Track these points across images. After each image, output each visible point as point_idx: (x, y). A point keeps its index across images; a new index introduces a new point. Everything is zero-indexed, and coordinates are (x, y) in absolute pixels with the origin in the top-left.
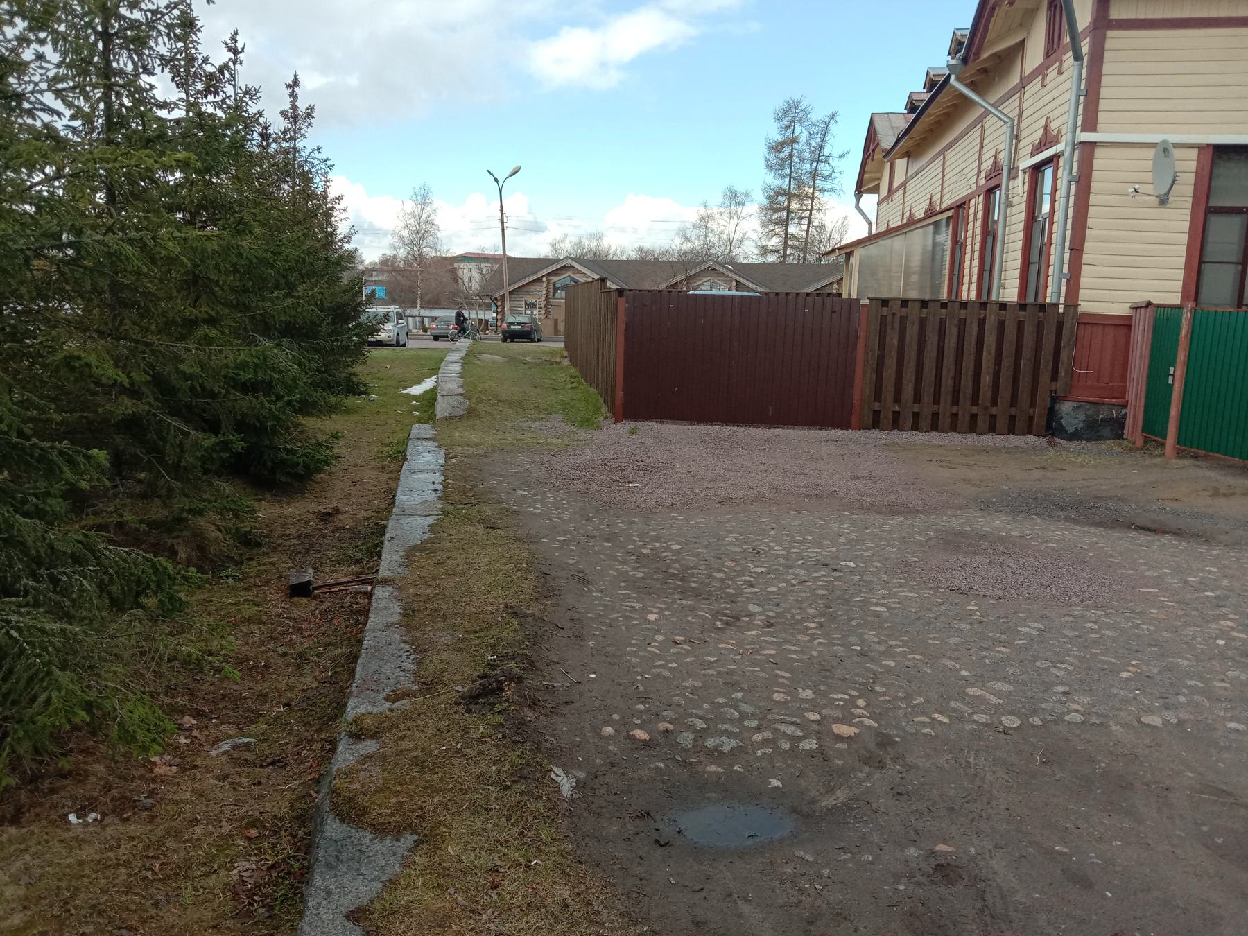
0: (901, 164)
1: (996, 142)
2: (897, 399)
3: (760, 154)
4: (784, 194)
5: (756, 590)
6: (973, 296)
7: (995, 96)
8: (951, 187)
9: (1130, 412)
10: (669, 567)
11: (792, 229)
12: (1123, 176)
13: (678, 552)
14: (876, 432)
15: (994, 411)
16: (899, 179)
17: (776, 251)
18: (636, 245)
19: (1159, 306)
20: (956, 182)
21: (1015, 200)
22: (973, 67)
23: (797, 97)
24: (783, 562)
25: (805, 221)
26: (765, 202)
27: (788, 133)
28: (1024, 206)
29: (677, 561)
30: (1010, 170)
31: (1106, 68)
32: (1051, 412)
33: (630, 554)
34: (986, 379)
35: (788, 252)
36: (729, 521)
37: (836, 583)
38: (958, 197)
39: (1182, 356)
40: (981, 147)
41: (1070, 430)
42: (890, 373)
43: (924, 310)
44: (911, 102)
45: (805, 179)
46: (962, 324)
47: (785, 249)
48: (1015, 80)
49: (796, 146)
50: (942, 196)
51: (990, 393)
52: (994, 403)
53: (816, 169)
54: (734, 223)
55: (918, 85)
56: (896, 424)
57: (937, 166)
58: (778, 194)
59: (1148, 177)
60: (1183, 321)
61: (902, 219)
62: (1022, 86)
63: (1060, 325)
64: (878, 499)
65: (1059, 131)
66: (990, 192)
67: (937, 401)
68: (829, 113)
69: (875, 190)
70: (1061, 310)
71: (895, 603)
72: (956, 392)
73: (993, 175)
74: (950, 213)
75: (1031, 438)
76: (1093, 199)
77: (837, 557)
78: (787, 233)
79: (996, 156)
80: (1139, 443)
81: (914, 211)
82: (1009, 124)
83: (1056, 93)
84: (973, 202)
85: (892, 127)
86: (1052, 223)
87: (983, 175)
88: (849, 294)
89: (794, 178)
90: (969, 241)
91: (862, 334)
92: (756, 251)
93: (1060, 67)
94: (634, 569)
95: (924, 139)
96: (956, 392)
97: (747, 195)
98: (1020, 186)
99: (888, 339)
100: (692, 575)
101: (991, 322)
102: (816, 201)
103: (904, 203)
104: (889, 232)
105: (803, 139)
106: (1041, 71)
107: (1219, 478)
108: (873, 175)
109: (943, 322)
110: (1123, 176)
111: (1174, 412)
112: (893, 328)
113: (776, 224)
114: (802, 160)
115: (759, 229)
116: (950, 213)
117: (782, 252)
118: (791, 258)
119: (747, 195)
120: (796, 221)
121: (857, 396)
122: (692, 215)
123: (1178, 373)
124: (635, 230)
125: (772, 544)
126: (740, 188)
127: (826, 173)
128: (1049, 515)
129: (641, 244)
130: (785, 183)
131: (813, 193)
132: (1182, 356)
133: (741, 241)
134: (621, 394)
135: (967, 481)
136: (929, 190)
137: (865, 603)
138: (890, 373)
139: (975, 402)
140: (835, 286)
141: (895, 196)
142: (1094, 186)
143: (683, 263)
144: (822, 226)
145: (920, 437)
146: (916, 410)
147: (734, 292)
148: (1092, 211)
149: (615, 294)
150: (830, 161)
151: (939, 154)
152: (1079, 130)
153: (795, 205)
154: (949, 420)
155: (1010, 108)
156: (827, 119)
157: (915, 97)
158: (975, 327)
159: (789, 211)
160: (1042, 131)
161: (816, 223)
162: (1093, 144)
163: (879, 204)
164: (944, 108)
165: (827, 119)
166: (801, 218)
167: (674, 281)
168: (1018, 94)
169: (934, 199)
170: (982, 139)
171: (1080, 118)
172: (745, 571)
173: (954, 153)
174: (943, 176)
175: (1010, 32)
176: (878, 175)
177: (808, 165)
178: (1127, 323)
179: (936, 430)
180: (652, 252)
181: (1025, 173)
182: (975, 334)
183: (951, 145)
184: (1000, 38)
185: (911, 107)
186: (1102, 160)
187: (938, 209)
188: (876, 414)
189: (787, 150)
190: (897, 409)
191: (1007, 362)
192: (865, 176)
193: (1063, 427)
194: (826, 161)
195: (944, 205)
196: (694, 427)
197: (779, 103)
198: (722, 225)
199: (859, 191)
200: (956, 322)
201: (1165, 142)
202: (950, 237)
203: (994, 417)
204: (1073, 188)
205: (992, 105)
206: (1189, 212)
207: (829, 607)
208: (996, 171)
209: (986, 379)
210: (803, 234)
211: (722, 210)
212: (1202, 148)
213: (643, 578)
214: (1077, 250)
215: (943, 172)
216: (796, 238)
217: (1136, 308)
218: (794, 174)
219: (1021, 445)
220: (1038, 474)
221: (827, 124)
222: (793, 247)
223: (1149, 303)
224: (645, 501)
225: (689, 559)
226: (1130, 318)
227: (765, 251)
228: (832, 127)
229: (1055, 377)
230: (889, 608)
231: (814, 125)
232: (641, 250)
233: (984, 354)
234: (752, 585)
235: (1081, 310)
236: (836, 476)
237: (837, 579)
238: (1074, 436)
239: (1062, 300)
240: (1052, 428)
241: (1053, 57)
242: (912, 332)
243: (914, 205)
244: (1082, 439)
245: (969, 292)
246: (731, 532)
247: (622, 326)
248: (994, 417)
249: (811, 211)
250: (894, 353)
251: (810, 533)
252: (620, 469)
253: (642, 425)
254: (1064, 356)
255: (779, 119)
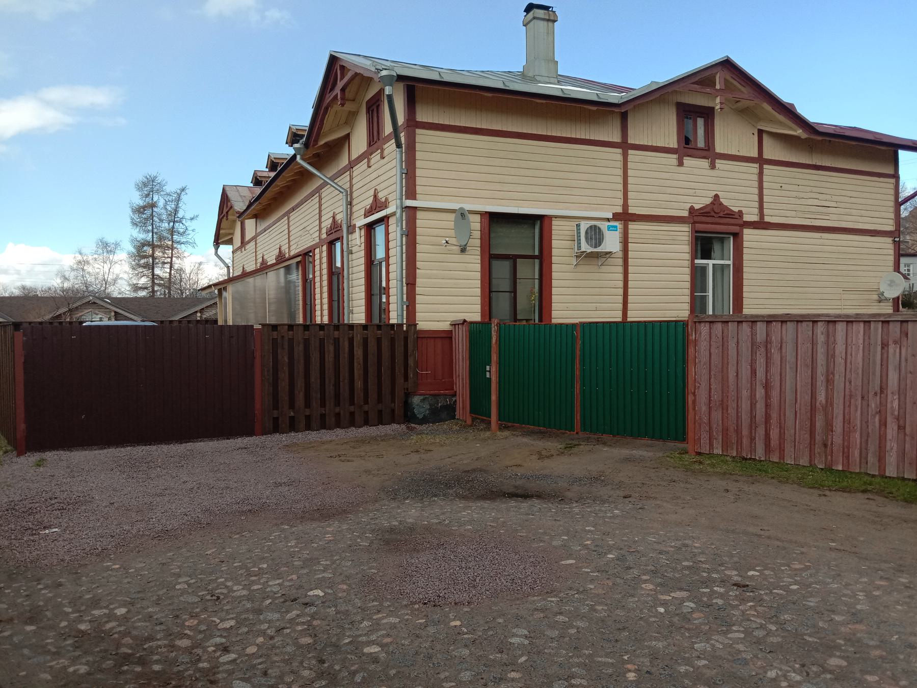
0: (250, 224)
1: (332, 207)
2: (292, 406)
3: (127, 214)
4: (149, 245)
5: (233, 656)
6: (326, 320)
7: (333, 170)
8: (297, 240)
9: (459, 399)
10: (118, 645)
11: (157, 271)
12: (436, 232)
13: (125, 618)
14: (277, 436)
15: (366, 408)
16: (249, 235)
17: (146, 288)
18: (19, 284)
19: (471, 323)
20: (301, 236)
21: (354, 249)
22: (311, 152)
23: (154, 174)
24: (249, 605)
25: (168, 266)
26: (134, 250)
27: (148, 200)
28: (362, 253)
29: (126, 634)
30: (348, 227)
31: (418, 155)
32: (407, 405)
33: (63, 636)
34: (359, 384)
35: (156, 289)
36: (172, 560)
37: (315, 623)
38: (304, 247)
39: (494, 357)
40: (320, 211)
41: (420, 416)
42: (284, 385)
43: (307, 332)
44: (256, 178)
45: (165, 234)
46: (337, 342)
47: (153, 287)
48: (344, 162)
49: (155, 209)
50: (289, 247)
51: (362, 395)
52: (366, 402)
53: (173, 227)
54: (107, 267)
55: (262, 166)
56: (293, 427)
57: (283, 224)
58: (143, 245)
59: (452, 233)
60: (493, 333)
61: (256, 264)
62: (351, 165)
63: (406, 339)
64: (307, 505)
65: (386, 199)
66: (331, 244)
67: (323, 405)
68: (180, 187)
69: (230, 242)
70: (405, 329)
71: (383, 636)
72: (337, 396)
73: (333, 231)
74: (299, 259)
75: (395, 426)
76: (419, 248)
77: (301, 587)
78: (153, 274)
79: (334, 218)
80: (469, 422)
81: (265, 257)
82: (344, 194)
83: (380, 172)
84: (317, 251)
85: (241, 196)
86: (388, 265)
87: (324, 231)
88: (226, 321)
89: (156, 233)
90: (317, 279)
91: (258, 354)
92: (128, 288)
93: (382, 153)
94: (74, 661)
95: (269, 205)
96: (337, 396)
97: (117, 245)
98: (358, 239)
99: (280, 357)
100: (152, 651)
101: (358, 340)
102: (175, 251)
103: (256, 252)
104: (245, 275)
105: (161, 203)
106: (366, 156)
107: (532, 442)
108: (227, 231)
109: (322, 341)
110: (436, 232)
111: (494, 398)
112: (283, 348)
113: (144, 267)
114: (161, 221)
115: (131, 271)
116: (299, 259)
117: (151, 289)
118: (159, 293)
119: (117, 245)
120: (160, 265)
121: (258, 406)
122: (68, 260)
123: (494, 369)
124: (18, 272)
125: (229, 584)
126: (110, 239)
127: (182, 231)
128: (444, 495)
129: (24, 283)
130: (149, 237)
131: (172, 245)
132: (494, 357)
133: (115, 281)
134: (22, 426)
135: (368, 472)
136: (277, 242)
137: (356, 645)
138: (284, 385)
139: (352, 402)
140: (199, 314)
141: (247, 247)
142: (419, 239)
143: (65, 298)
144: (180, 271)
145: (313, 436)
146: (307, 414)
147: (113, 323)
148: (419, 256)
149: (10, 330)
150: (184, 222)
151: (284, 216)
152: (404, 197)
153: (158, 253)
154: (333, 419)
155: (344, 180)
156: (179, 191)
157: (259, 174)
158: (346, 344)
159: (154, 258)
160: (372, 199)
161: (176, 266)
162: (415, 208)
163: (233, 252)
164: (288, 182)
165: (179, 191)
166: (164, 263)
167: (58, 313)
168: (348, 173)
169: (283, 249)
170: (320, 206)
171: (404, 189)
172: (212, 626)
173: (297, 214)
174: (289, 232)
175: (338, 127)
176: (231, 231)
177: (166, 225)
178: (450, 336)
179: (325, 428)
180: (35, 290)
181: (360, 229)
182: (347, 350)
183: (293, 209)
184: (331, 131)
185: (257, 181)
186: (422, 220)
187: (287, 256)
188: (276, 420)
189: (148, 212)
190: (292, 414)
191: (372, 370)
192: (221, 231)
193: (415, 415)
194: (180, 222)
195: (292, 253)
196: (105, 451)
197: (140, 177)
198: (97, 270)
199: (217, 242)
200: (332, 341)
201: (461, 209)
202: (300, 277)
203: (366, 413)
204: (404, 239)
205: (329, 179)
206: (479, 257)
207: (322, 662)
208: (335, 227)
209: (359, 384)
210: (167, 275)
211: (96, 256)
212: (483, 214)
213: (89, 674)
214: (411, 284)
215: (289, 228)
216: (162, 279)
217: (455, 325)
218: (155, 230)
219: (389, 432)
220: (415, 458)
221: (179, 196)
222: (159, 285)
223: (465, 321)
224: (69, 551)
225: (142, 627)
226: (449, 332)
227: (136, 288)
228: (183, 197)
229: (406, 378)
230: (382, 646)
231: (168, 194)
232: (24, 288)
233: (355, 364)
234: (226, 650)
235: (418, 327)
236: (260, 486)
237: (313, 616)
238: (424, 421)
239: (405, 321)
240: (408, 417)
241: (375, 146)
242: (299, 349)
243: (265, 253)
244: (429, 422)
245: (322, 316)
246: (179, 576)
247: (20, 360)
248: (366, 413)
249: (171, 258)
250: (286, 369)
251: (263, 559)
252: (31, 512)
253: (49, 455)
254: (411, 362)
255: (139, 189)
